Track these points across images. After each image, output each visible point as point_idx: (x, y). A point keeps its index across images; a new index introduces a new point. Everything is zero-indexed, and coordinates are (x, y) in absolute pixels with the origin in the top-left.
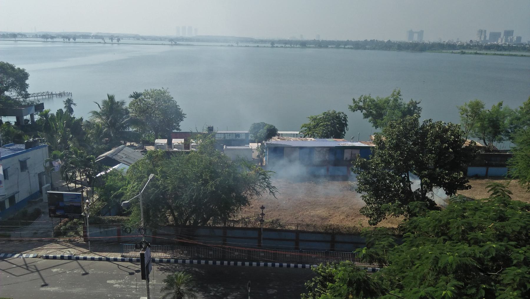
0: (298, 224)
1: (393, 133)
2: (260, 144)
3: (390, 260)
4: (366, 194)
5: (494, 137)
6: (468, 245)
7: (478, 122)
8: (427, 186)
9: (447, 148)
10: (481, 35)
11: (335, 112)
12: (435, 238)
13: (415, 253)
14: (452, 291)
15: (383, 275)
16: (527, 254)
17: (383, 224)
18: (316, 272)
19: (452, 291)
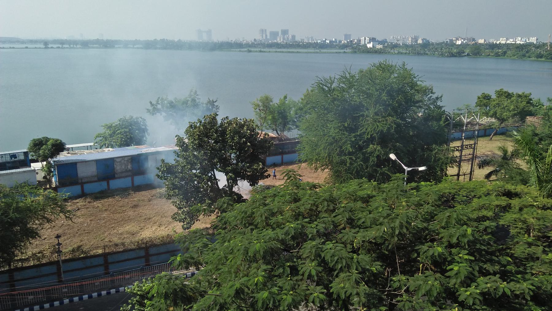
0: (104, 246)
1: (194, 134)
2: (45, 163)
3: (206, 260)
4: (176, 199)
5: (284, 127)
6: (271, 230)
7: (269, 115)
8: (232, 181)
9: (245, 143)
10: (263, 33)
11: (132, 118)
12: (244, 229)
13: (227, 248)
14: (263, 276)
15: (201, 278)
16: (318, 227)
17: (198, 225)
18: (131, 292)
19: (263, 276)
